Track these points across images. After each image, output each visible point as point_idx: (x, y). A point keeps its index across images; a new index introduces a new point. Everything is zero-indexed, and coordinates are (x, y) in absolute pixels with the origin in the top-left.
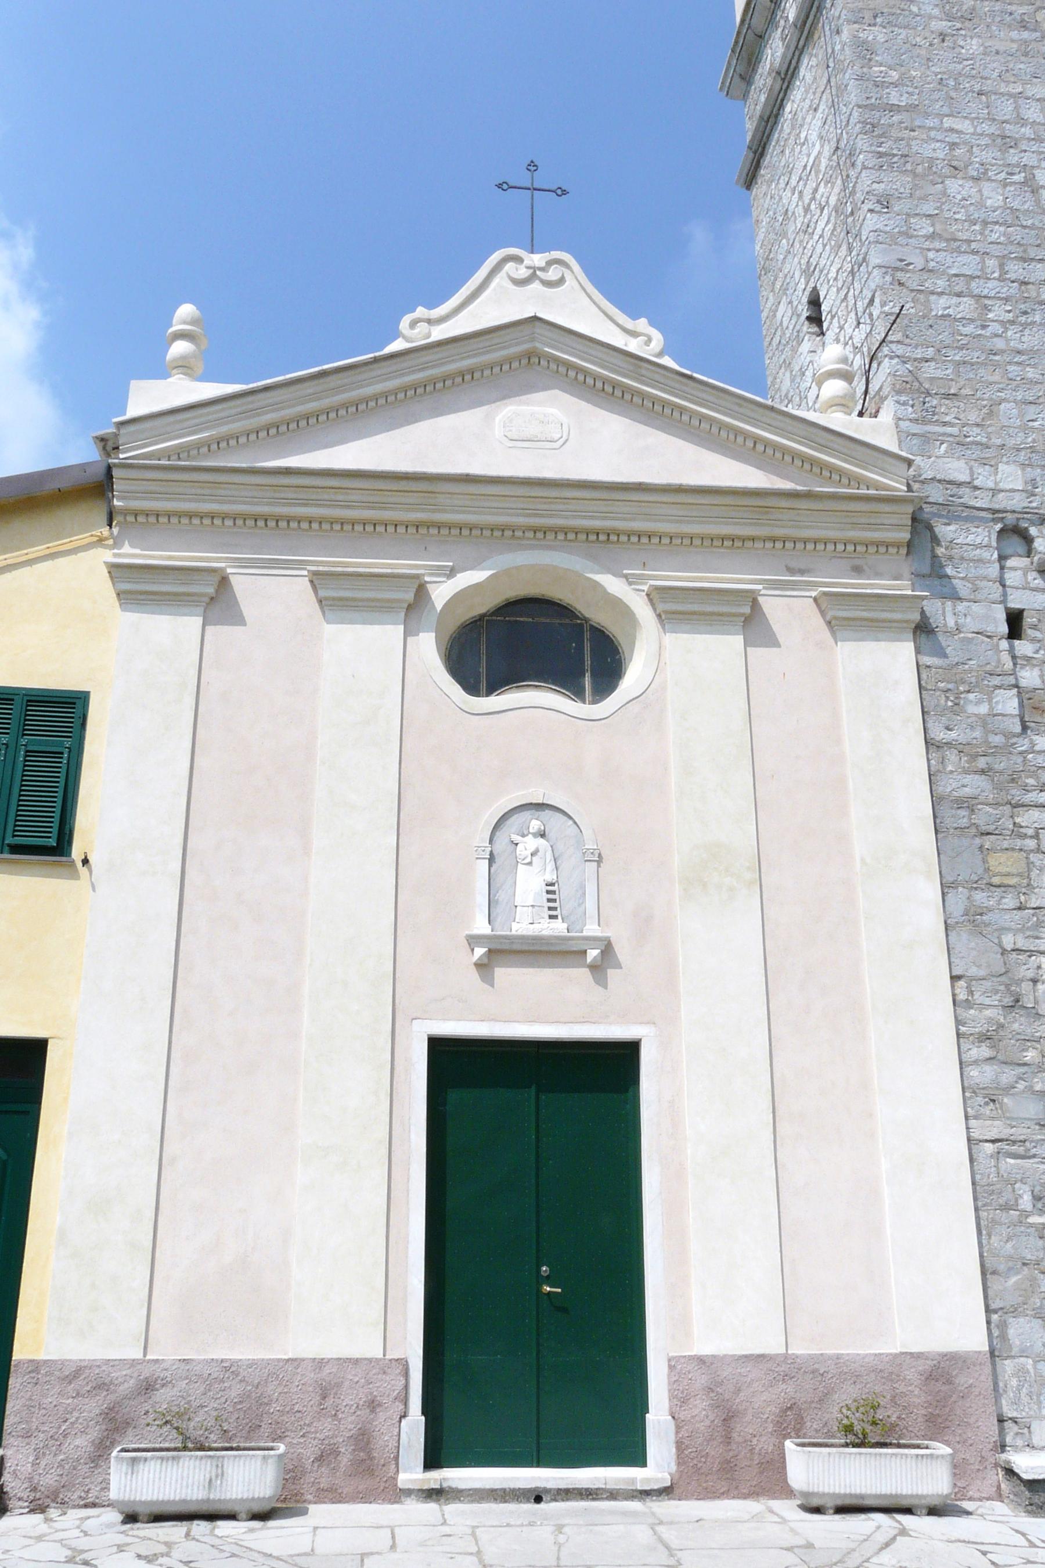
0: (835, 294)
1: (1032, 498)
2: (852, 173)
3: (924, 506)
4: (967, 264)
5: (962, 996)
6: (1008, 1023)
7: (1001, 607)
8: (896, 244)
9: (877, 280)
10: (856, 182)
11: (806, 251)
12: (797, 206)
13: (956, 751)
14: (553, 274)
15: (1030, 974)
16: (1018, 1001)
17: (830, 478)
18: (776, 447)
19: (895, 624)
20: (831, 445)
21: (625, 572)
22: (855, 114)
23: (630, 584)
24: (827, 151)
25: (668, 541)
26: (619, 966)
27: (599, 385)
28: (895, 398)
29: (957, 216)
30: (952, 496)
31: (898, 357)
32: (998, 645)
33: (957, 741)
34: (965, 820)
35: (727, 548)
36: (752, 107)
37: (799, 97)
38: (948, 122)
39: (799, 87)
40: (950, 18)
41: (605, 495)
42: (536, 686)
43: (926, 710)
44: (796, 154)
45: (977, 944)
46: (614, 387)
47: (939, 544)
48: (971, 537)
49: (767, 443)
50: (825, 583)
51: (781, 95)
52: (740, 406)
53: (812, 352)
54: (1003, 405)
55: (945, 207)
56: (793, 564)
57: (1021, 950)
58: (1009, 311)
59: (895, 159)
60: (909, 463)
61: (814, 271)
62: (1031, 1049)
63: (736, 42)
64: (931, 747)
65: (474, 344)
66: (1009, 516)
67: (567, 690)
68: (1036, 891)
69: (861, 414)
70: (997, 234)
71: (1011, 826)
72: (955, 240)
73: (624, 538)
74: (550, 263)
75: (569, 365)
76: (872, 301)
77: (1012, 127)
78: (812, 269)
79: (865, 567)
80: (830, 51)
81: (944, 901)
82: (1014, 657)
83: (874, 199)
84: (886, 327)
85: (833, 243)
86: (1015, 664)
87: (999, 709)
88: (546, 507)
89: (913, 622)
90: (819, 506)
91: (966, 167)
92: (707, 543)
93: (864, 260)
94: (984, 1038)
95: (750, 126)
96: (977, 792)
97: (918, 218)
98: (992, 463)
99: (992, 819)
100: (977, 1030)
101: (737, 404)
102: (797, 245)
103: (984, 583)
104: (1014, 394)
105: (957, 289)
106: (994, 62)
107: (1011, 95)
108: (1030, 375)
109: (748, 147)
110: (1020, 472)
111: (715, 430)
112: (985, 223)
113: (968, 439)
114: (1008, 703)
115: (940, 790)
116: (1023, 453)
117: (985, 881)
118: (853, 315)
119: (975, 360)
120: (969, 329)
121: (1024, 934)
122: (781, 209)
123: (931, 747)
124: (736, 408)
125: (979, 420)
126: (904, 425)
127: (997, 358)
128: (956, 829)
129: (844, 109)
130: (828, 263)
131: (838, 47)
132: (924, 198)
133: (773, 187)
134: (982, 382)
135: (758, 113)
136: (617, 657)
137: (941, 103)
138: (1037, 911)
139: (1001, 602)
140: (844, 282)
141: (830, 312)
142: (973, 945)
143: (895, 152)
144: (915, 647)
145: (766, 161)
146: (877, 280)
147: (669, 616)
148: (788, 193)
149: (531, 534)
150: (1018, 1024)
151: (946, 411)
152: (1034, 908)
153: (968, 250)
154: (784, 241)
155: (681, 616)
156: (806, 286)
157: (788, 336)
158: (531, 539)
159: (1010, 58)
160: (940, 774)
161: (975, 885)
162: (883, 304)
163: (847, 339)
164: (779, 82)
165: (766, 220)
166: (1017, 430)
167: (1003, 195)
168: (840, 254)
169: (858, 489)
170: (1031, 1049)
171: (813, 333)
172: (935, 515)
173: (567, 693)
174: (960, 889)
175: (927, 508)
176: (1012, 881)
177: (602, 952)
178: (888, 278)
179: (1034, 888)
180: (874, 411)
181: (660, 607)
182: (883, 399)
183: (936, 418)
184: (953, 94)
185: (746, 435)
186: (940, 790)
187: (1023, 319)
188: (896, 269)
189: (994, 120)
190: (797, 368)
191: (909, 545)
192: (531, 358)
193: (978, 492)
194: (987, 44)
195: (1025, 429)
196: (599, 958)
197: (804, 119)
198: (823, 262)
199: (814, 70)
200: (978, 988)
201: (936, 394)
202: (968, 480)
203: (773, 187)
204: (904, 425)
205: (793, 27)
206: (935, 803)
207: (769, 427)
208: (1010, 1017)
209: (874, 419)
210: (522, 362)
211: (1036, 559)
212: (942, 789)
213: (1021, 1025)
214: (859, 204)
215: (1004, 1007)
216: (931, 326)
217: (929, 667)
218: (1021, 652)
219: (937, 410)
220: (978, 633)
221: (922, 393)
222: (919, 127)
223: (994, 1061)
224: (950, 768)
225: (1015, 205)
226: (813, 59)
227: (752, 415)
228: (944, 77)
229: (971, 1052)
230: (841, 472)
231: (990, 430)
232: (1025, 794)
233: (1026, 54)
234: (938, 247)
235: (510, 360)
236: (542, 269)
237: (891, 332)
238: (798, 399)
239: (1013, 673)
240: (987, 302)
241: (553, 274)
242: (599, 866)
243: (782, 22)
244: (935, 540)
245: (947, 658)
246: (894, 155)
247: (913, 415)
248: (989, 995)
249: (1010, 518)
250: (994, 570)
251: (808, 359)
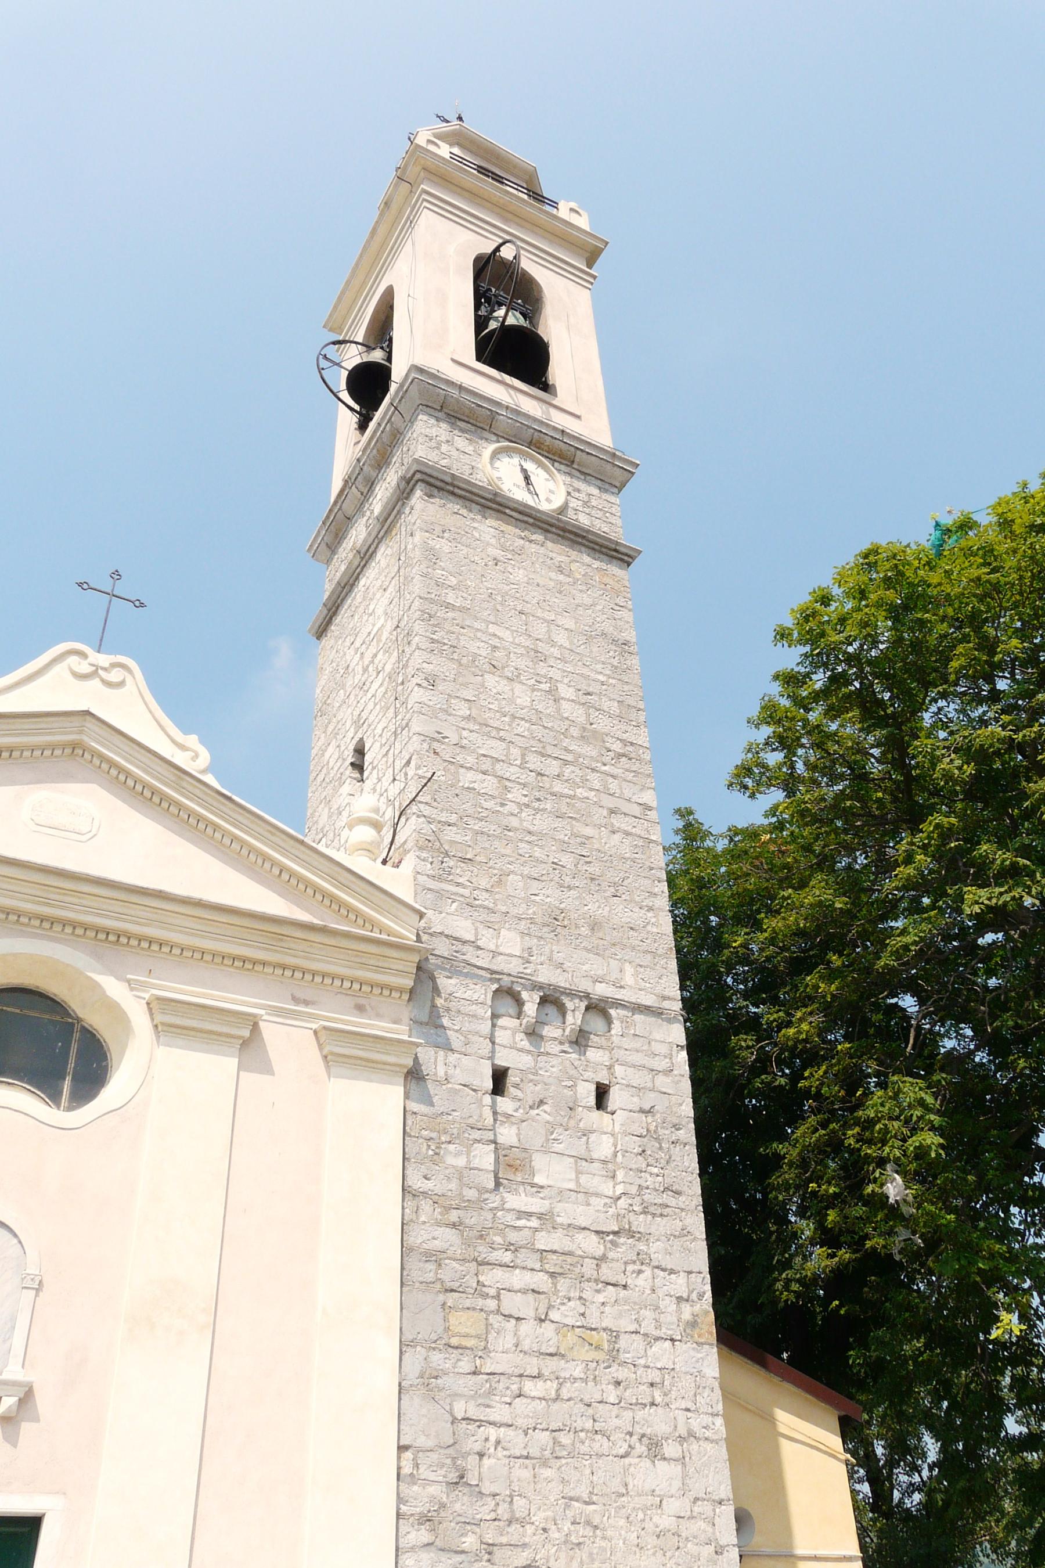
0: (378, 749)
1: (527, 965)
2: (407, 649)
3: (430, 957)
4: (496, 749)
5: (407, 1470)
6: (451, 1502)
7: (489, 1063)
8: (436, 717)
9: (415, 745)
10: (409, 658)
11: (359, 705)
12: (357, 664)
13: (431, 1202)
14: (115, 676)
15: (477, 1447)
16: (462, 1477)
17: (347, 916)
18: (300, 879)
19: (388, 1067)
20: (353, 886)
21: (129, 976)
22: (417, 603)
23: (132, 989)
24: (390, 625)
25: (178, 951)
26: (37, 1419)
27: (139, 788)
28: (417, 853)
29: (491, 706)
30: (456, 952)
31: (425, 816)
32: (481, 1100)
33: (433, 1191)
34: (432, 1274)
35: (237, 968)
36: (333, 572)
37: (372, 576)
38: (492, 629)
39: (374, 568)
40: (504, 549)
41: (122, 896)
42: (9, 1084)
43: (407, 1156)
44: (363, 621)
45: (429, 1410)
46: (153, 793)
47: (439, 995)
48: (469, 993)
49: (292, 874)
50: (324, 1016)
51: (359, 570)
52: (273, 834)
53: (351, 795)
54: (511, 876)
55: (482, 696)
56: (299, 994)
57: (471, 1420)
58: (526, 796)
59: (445, 647)
60: (422, 915)
61: (363, 724)
62: (470, 1533)
63: (328, 517)
64: (407, 1195)
65: (19, 724)
66: (505, 978)
67: (42, 1092)
68: (492, 1355)
69: (384, 862)
70: (523, 729)
71: (475, 1285)
72: (487, 726)
73: (134, 942)
74: (114, 665)
75: (112, 764)
76: (408, 762)
77: (543, 645)
78: (362, 722)
79: (368, 1007)
80: (403, 547)
81: (401, 1360)
82: (495, 1113)
83: (423, 676)
84: (417, 788)
85: (383, 704)
86: (495, 1120)
87: (476, 1163)
88: (57, 897)
89: (405, 1066)
90: (332, 941)
91: (503, 668)
92: (218, 960)
93: (407, 725)
94: (425, 1519)
95: (328, 588)
96: (445, 1246)
97: (458, 700)
98: (496, 927)
99: (458, 1275)
100: (418, 1509)
101: (270, 832)
102: (352, 697)
103: (476, 1038)
104: (522, 868)
105: (484, 767)
106: (535, 591)
107: (545, 621)
108: (537, 854)
109: (324, 604)
110: (519, 939)
111: (244, 852)
112: (514, 717)
113: (477, 902)
114: (485, 1158)
115: (410, 1240)
116: (523, 922)
117: (444, 1342)
118: (391, 770)
119: (492, 832)
120: (490, 804)
121: (476, 1401)
122: (344, 665)
123: (407, 1195)
124: (266, 834)
125: (488, 887)
126: (421, 879)
127: (511, 834)
128: (421, 1283)
129: (408, 595)
130: (377, 721)
131: (410, 547)
132: (465, 685)
133: (340, 642)
134: (496, 853)
135: (337, 578)
136: (104, 1064)
137: (489, 612)
138: (491, 1377)
139: (489, 1058)
140: (388, 740)
141: (372, 763)
142: (424, 1411)
143: (446, 641)
144: (405, 1092)
145: (338, 620)
146: (415, 745)
147: (165, 1028)
148: (352, 651)
149: (37, 923)
150: (461, 1504)
151: (461, 873)
152: (488, 1374)
153: (497, 736)
154: (342, 691)
155: (179, 1031)
156: (355, 735)
157: (332, 775)
158: (229, 966)
159: (547, 592)
160: (412, 1224)
161: (433, 1345)
162: (418, 768)
163: (383, 790)
164: (359, 560)
165: (329, 669)
166: (521, 901)
167: (530, 697)
168: (387, 715)
169: (372, 931)
170: (470, 1533)
171: (355, 779)
172: (438, 967)
173: (42, 1095)
174: (419, 1348)
175: (432, 960)
176: (470, 1343)
177: (20, 1400)
178: (425, 746)
179: (490, 1352)
180: (397, 861)
181: (159, 1018)
182: (408, 852)
183: (451, 877)
184: (499, 608)
185: (274, 863)
186: (410, 1240)
187: (536, 805)
188: (433, 739)
189: (530, 636)
190: (335, 807)
191: (412, 991)
192: (76, 749)
193: (480, 952)
194: (530, 576)
195: (529, 902)
196: (15, 1408)
197: (374, 594)
198: (372, 718)
199: (388, 558)
200: (424, 1460)
201: (453, 856)
202: (473, 939)
203: (340, 642)
204: (421, 879)
205: (376, 521)
206: (404, 1255)
207: (297, 859)
208: (453, 1495)
209: (396, 869)
210: (65, 751)
211: (524, 1021)
212: (414, 1239)
213: (463, 1505)
214: (410, 676)
215: (448, 1484)
216: (457, 795)
217: (415, 1113)
218: (502, 1109)
219: (453, 871)
220: (464, 1085)
221: (442, 853)
222: (469, 626)
223: (433, 1548)
224: (423, 1218)
225: (540, 708)
226: (389, 549)
227: (282, 844)
228: (493, 592)
229: (409, 1536)
230: (358, 914)
231: (497, 897)
232: (491, 1252)
233: (560, 592)
234: (471, 728)
235: (53, 747)
236: (105, 669)
237: (421, 794)
238: (332, 835)
239: (493, 1129)
240: (507, 783)
241: (115, 676)
242: (37, 1295)
243: (368, 513)
244: (436, 990)
245: (434, 1106)
246: (445, 644)
247: (431, 872)
248: (435, 1469)
249: (506, 981)
250: (486, 1027)
251: (346, 801)
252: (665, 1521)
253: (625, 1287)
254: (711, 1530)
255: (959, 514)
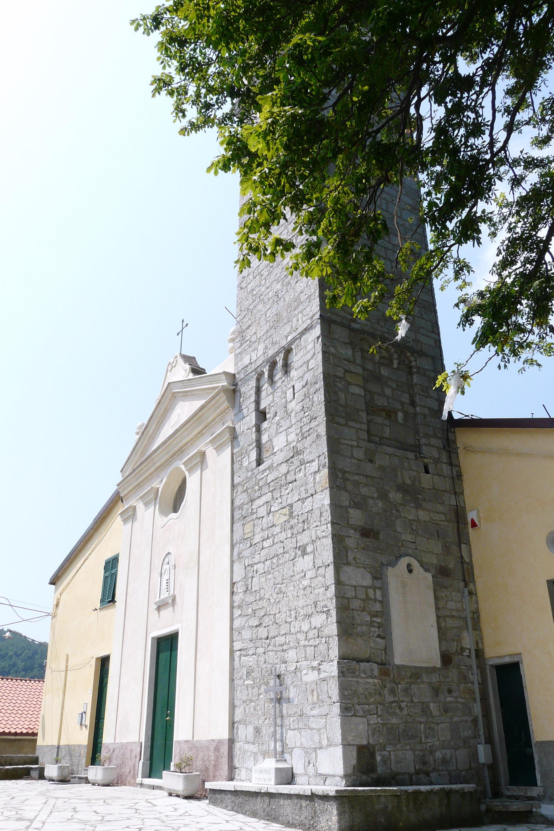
252: (306, 583)
253: (295, 480)
254: (323, 580)
255: (538, 85)
